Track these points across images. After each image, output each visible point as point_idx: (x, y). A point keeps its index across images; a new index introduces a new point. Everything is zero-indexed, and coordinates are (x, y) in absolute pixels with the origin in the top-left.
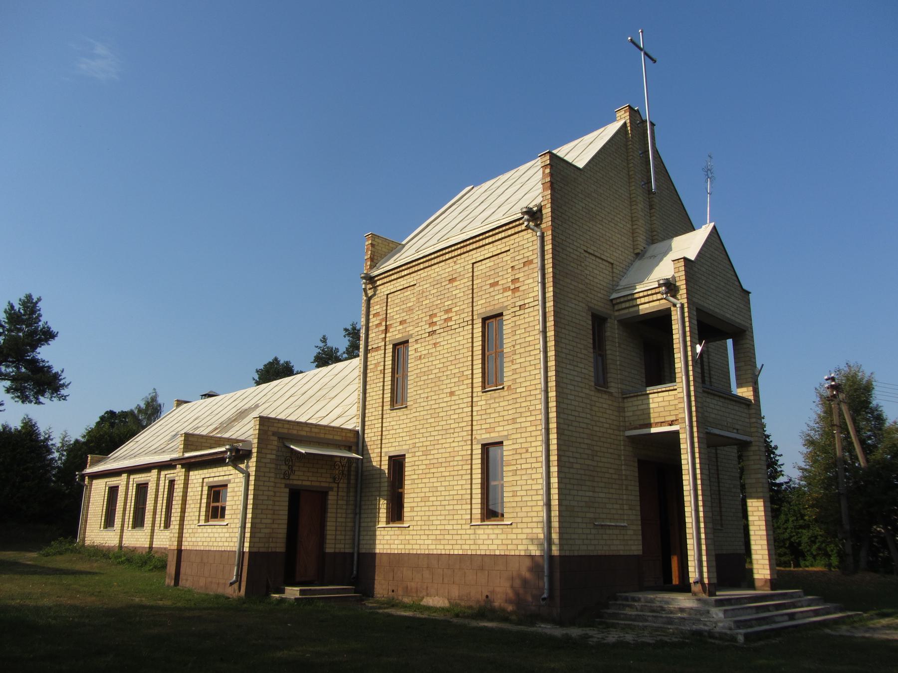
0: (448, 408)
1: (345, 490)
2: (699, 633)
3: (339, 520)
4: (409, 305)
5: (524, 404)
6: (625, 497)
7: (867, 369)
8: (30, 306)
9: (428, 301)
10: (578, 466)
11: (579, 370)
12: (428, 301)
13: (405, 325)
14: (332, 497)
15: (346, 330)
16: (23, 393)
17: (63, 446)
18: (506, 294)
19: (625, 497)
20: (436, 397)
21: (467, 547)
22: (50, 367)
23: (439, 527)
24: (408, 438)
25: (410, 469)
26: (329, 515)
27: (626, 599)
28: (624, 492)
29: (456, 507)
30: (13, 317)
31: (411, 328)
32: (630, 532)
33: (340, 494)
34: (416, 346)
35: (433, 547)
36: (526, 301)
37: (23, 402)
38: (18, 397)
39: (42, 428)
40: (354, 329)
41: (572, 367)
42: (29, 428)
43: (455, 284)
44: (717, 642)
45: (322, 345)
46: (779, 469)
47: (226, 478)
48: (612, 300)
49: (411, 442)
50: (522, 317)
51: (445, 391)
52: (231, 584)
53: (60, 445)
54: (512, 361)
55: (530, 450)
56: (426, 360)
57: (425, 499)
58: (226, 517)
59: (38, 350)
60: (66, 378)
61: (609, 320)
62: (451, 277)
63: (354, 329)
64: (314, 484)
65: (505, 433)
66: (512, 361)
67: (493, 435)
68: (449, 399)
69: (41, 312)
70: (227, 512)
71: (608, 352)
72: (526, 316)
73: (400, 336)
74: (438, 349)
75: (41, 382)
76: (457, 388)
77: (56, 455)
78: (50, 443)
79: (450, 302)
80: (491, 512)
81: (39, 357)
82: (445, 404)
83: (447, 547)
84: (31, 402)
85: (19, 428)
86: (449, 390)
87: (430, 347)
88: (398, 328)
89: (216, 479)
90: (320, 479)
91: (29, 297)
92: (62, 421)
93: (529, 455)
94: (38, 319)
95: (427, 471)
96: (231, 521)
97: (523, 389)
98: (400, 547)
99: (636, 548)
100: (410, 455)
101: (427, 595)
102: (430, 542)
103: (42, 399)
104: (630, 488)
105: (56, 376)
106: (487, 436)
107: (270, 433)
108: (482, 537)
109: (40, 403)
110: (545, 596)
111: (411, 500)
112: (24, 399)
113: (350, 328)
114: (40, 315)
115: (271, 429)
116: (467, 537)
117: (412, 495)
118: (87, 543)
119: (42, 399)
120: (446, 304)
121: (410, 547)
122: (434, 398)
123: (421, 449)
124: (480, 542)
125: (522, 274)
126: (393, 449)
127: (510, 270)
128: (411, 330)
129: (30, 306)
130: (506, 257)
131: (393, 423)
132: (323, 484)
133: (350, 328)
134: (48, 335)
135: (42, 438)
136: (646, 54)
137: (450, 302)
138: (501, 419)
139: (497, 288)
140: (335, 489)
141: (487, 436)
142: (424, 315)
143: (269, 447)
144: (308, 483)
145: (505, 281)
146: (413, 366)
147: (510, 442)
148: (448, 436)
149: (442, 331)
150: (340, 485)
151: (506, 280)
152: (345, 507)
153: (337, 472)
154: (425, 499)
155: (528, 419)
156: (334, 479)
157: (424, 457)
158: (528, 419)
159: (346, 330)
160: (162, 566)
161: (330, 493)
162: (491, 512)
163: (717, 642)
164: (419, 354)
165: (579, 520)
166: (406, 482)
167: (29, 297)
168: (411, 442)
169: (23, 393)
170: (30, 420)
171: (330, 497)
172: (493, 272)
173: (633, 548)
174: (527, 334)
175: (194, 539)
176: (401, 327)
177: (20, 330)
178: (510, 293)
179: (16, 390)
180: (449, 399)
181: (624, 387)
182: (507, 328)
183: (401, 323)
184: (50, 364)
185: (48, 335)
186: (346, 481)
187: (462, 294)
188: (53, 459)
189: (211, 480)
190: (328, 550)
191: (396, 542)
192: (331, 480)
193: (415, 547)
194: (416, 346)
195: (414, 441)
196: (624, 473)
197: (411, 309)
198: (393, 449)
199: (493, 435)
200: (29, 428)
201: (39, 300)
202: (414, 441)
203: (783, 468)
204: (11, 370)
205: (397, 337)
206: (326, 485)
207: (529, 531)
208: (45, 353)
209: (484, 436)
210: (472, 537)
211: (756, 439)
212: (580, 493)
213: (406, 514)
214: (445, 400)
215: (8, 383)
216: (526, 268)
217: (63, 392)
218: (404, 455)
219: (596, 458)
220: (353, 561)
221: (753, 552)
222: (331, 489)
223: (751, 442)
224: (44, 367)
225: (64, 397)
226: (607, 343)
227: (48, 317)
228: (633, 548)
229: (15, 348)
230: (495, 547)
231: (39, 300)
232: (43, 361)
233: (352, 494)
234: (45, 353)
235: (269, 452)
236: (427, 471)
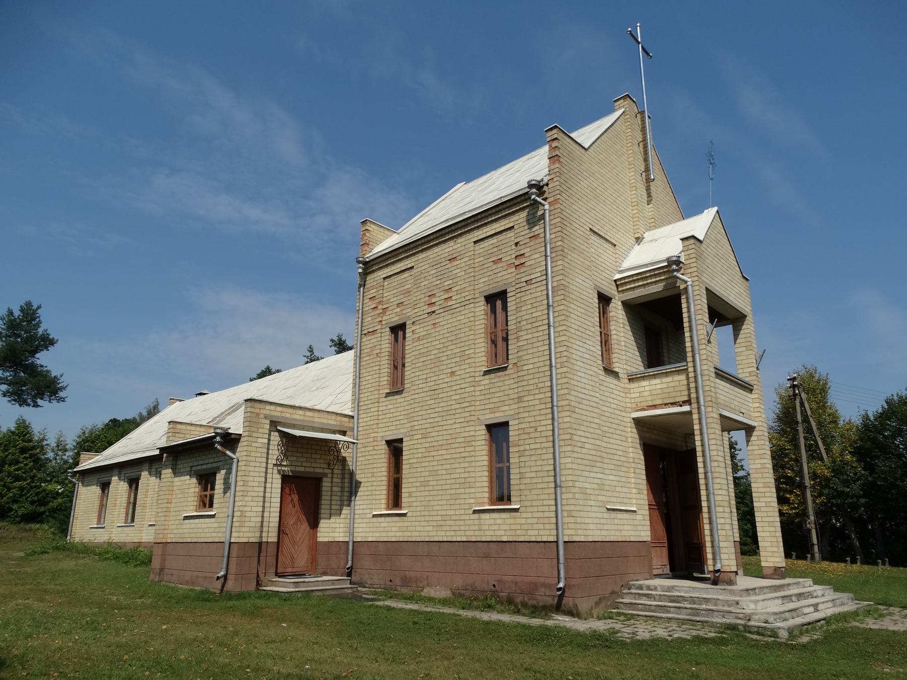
0: (449, 389)
1: (340, 476)
2: (733, 627)
3: (333, 507)
4: (406, 287)
5: (531, 382)
6: (633, 480)
7: (822, 371)
8: (30, 314)
9: (426, 283)
10: (589, 446)
11: (587, 347)
12: (426, 283)
13: (402, 308)
14: (326, 484)
15: (332, 341)
16: (20, 396)
17: (58, 446)
18: (510, 271)
19: (633, 480)
20: (436, 378)
21: (471, 533)
22: (48, 371)
23: (440, 513)
24: (406, 421)
25: (408, 453)
26: (323, 502)
27: (640, 587)
28: (632, 475)
29: (458, 491)
30: (13, 325)
31: (409, 310)
32: (639, 517)
33: (335, 480)
34: (414, 328)
35: (434, 534)
36: (533, 276)
37: (20, 405)
38: (15, 400)
39: (37, 429)
40: (340, 340)
41: (581, 344)
42: (23, 430)
43: (456, 263)
44: (755, 637)
45: (309, 354)
46: (739, 464)
47: (215, 465)
48: (615, 281)
49: (408, 425)
50: (528, 292)
51: (445, 371)
52: (218, 578)
53: (55, 445)
54: (518, 338)
55: (539, 429)
56: (425, 341)
57: (425, 484)
58: (214, 506)
59: (37, 355)
60: (63, 381)
61: (613, 300)
62: (451, 257)
63: (340, 340)
64: (307, 470)
65: (512, 412)
66: (518, 338)
67: (497, 415)
68: (450, 379)
69: (41, 318)
70: (215, 501)
71: (613, 332)
72: (533, 291)
73: (397, 318)
74: (437, 329)
75: (44, 387)
76: (458, 368)
77: (51, 455)
78: (45, 443)
79: (450, 282)
80: (501, 494)
81: (38, 362)
82: (445, 385)
83: (448, 533)
84: (29, 405)
85: (13, 429)
86: (450, 371)
87: (430, 327)
88: (395, 311)
89: (204, 467)
90: (314, 465)
91: (29, 304)
92: (55, 424)
93: (538, 435)
94: (38, 325)
95: (427, 454)
96: (219, 510)
97: (531, 366)
98: (398, 534)
99: (645, 534)
100: (408, 439)
101: (428, 585)
102: (430, 528)
103: (40, 402)
104: (637, 471)
105: (55, 380)
106: (492, 416)
107: (262, 416)
108: (488, 522)
109: (38, 406)
110: (561, 585)
111: (410, 485)
112: (22, 402)
113: (336, 339)
114: (40, 322)
115: (262, 411)
116: (471, 522)
117: (411, 480)
118: (77, 540)
119: (40, 402)
120: (446, 284)
121: (409, 534)
122: (433, 379)
123: (420, 432)
124: (486, 527)
125: (528, 249)
126: (390, 433)
127: (514, 247)
128: (409, 312)
129: (30, 314)
130: (510, 234)
131: (390, 407)
132: (317, 470)
133: (336, 339)
134: (47, 342)
135: (36, 438)
136: (643, 48)
137: (450, 282)
138: (506, 398)
139: (500, 265)
140: (329, 475)
141: (492, 416)
142: (423, 296)
143: (261, 430)
144: (302, 469)
145: (509, 258)
146: (411, 346)
147: (517, 422)
148: (449, 417)
149: (442, 311)
150: (335, 471)
151: (509, 258)
152: (339, 494)
153: (332, 458)
154: (425, 484)
155: (537, 397)
156: (329, 464)
157: (424, 440)
158: (537, 397)
159: (332, 341)
160: (147, 561)
161: (324, 479)
162: (501, 494)
163: (755, 637)
164: (417, 336)
165: (592, 503)
166: (404, 467)
167: (29, 304)
168: (408, 425)
169: (20, 396)
170: (24, 421)
171: (324, 484)
172: (496, 249)
173: (643, 533)
174: (534, 310)
175: (181, 531)
176: (398, 310)
177: (19, 336)
178: (514, 270)
179: (12, 394)
180: (450, 379)
181: (629, 368)
182: (511, 306)
183: (398, 305)
184: (48, 368)
185: (47, 342)
186: (340, 467)
187: (463, 273)
188: (47, 459)
189: (199, 468)
190: (320, 540)
191: (394, 529)
192: (326, 466)
193: (414, 534)
194: (414, 328)
195: (412, 424)
196: (631, 455)
197: (408, 292)
198: (390, 433)
199: (497, 415)
200: (23, 430)
201: (39, 307)
202: (412, 424)
203: (743, 463)
204: (8, 374)
205: (394, 320)
206: (321, 471)
207: (518, 521)
208: (43, 359)
209: (487, 417)
210: (477, 522)
211: (760, 423)
212: (592, 475)
213: (404, 500)
214: (445, 380)
215: (4, 387)
216: (532, 243)
217: (62, 394)
218: (402, 439)
219: (605, 439)
220: (348, 549)
221: (759, 539)
222: (326, 475)
223: (755, 427)
224: (42, 371)
225: (62, 400)
226: (612, 323)
227: (48, 324)
228: (643, 533)
229: (12, 354)
230: (503, 533)
231: (39, 307)
232: (42, 366)
233: (346, 480)
234: (43, 359)
235: (260, 435)
236: (427, 454)
